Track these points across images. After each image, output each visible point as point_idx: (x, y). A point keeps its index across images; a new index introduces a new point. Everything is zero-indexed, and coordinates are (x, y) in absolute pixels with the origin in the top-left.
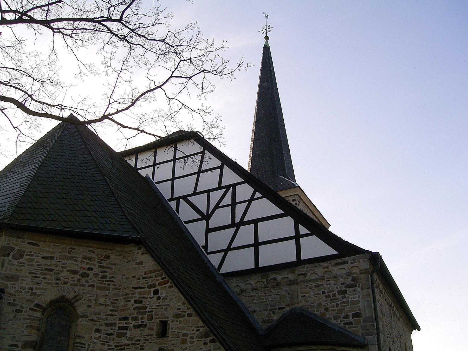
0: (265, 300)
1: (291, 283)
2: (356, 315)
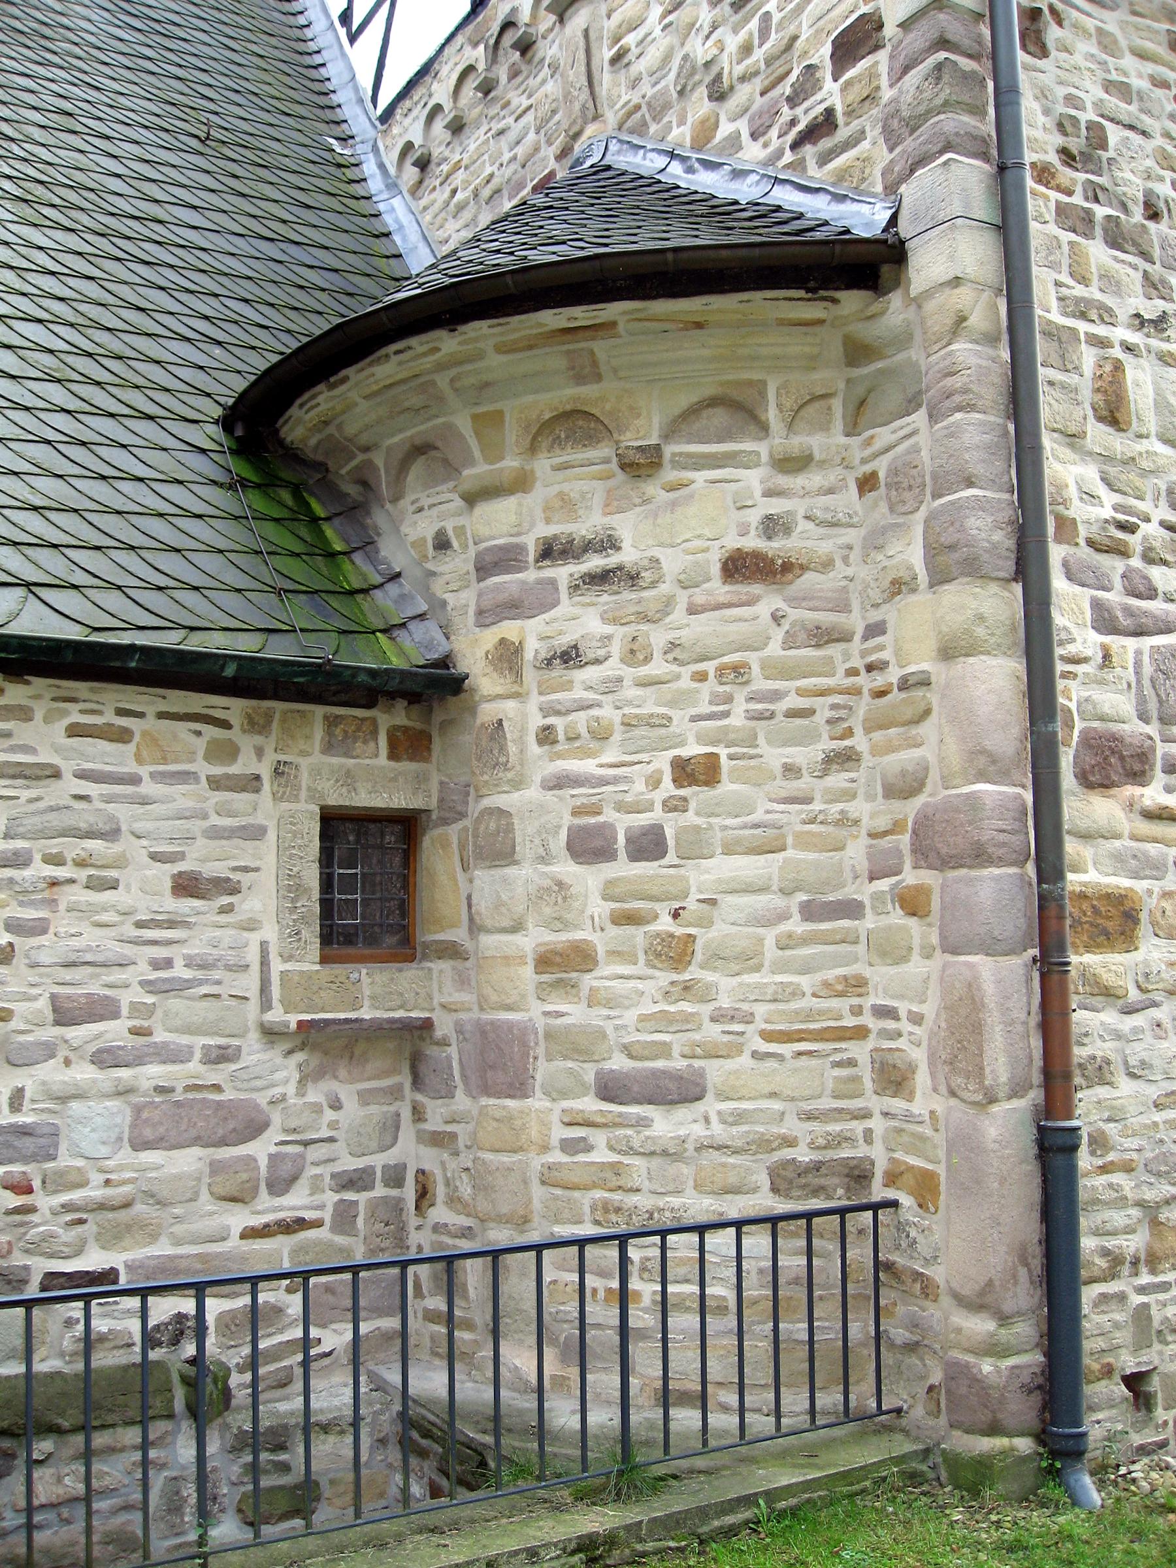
0: (488, 170)
2: (856, 41)
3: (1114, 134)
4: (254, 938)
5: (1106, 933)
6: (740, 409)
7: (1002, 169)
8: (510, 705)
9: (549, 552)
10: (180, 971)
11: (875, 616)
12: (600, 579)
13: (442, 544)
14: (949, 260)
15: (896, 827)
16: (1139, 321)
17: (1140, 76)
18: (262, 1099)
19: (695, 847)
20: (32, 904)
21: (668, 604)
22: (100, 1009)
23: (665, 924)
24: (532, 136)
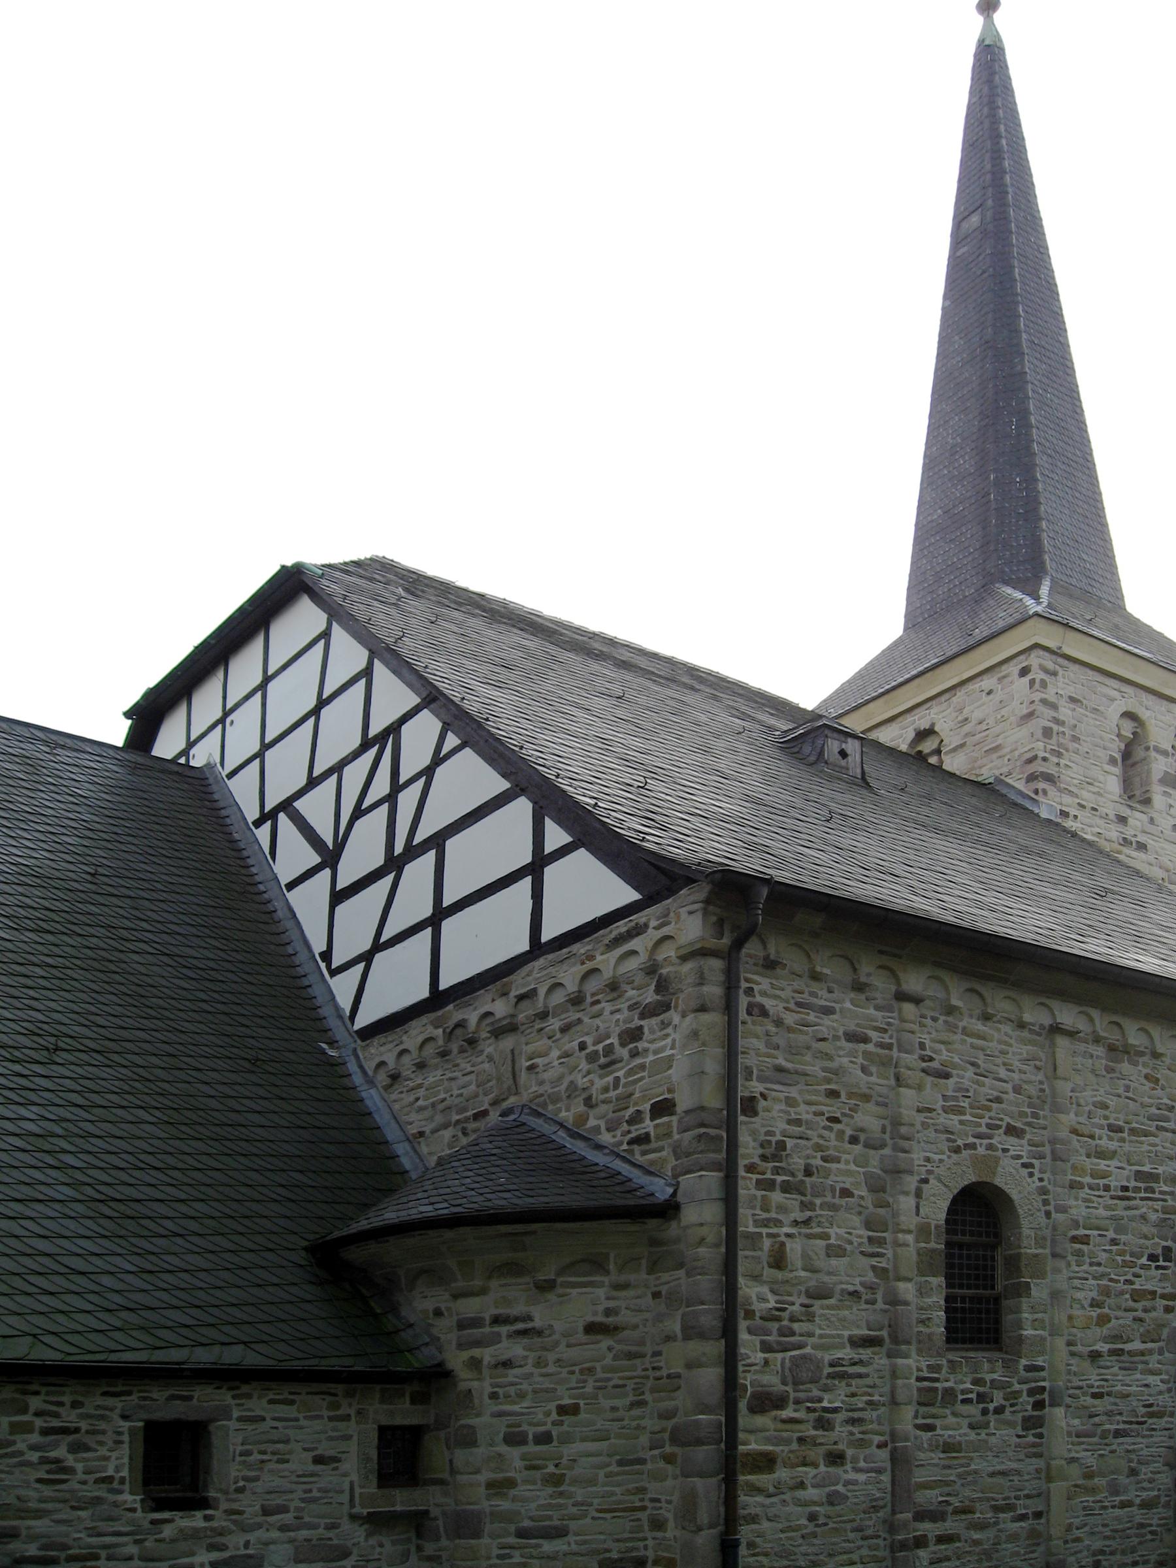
0: (442, 1096)
1: (509, 1028)
2: (663, 1108)
3: (790, 1143)
4: (347, 1480)
5: (759, 1467)
6: (597, 1264)
7: (727, 1177)
8: (475, 1384)
9: (497, 1320)
10: (315, 1494)
11: (657, 1348)
12: (524, 1333)
13: (438, 1313)
14: (700, 1215)
15: (663, 1430)
16: (796, 1223)
17: (808, 1113)
18: (349, 1544)
19: (566, 1439)
20: (253, 1470)
21: (557, 1343)
22: (283, 1509)
23: (551, 1469)
24: (473, 1087)
